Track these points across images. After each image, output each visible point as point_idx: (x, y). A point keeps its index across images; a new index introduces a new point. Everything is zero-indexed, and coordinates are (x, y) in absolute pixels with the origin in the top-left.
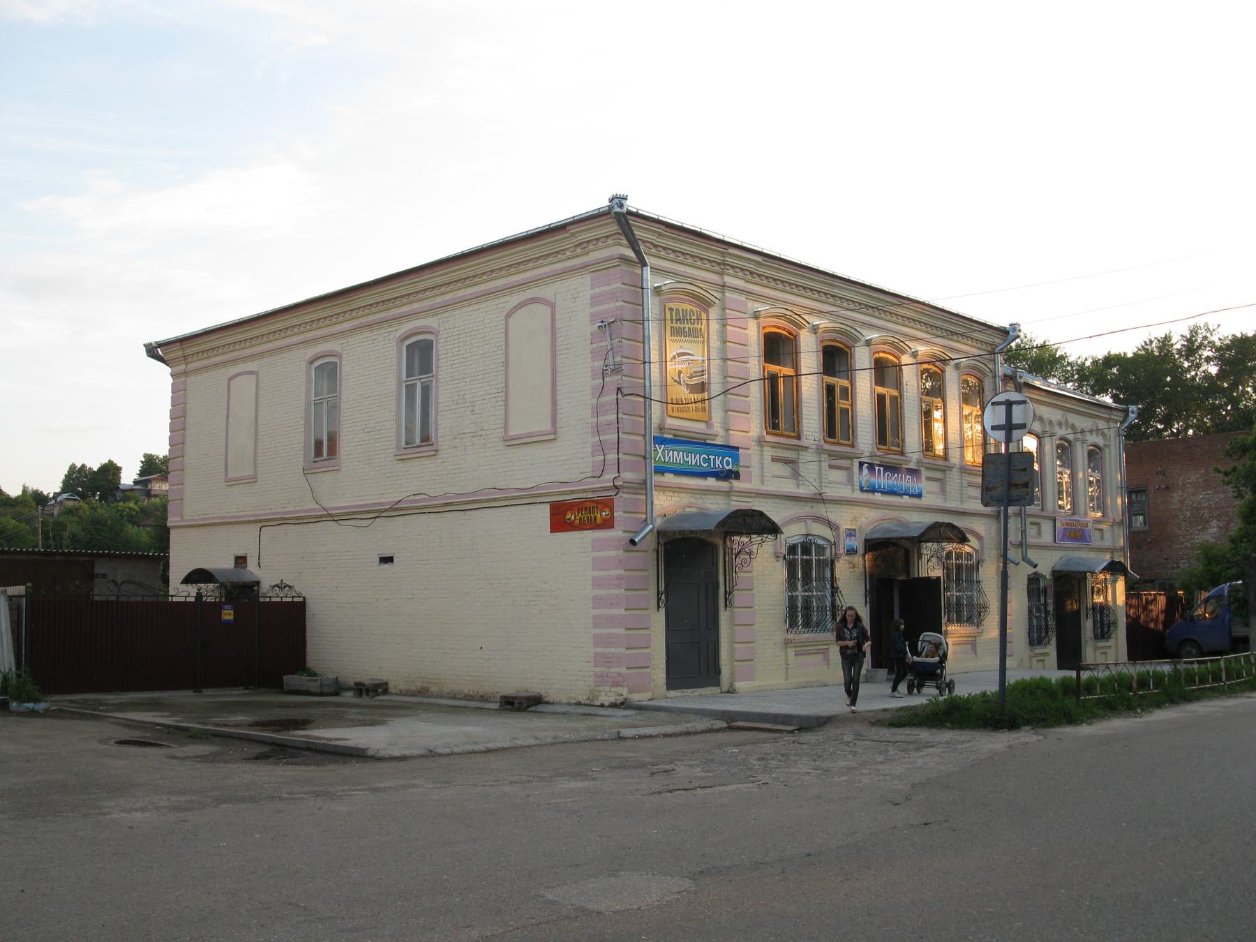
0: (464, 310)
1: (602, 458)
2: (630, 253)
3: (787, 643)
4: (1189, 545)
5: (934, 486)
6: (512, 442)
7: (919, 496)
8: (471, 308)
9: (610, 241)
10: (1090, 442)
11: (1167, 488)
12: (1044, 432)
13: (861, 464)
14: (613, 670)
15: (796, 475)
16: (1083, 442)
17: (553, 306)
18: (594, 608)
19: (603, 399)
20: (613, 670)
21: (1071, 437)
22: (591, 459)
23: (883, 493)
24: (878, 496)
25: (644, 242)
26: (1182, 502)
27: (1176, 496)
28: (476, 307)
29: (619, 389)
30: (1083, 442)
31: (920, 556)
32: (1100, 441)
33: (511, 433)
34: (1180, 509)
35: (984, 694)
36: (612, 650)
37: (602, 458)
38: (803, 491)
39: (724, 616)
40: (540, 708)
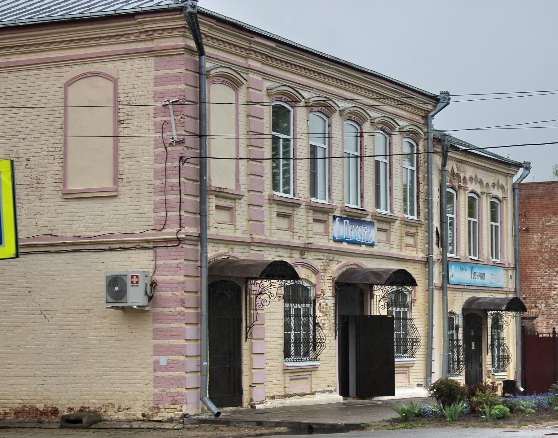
0: (18, 74)
1: (164, 214)
2: (192, 44)
3: (286, 370)
4: (547, 286)
5: (382, 236)
6: (71, 196)
7: (372, 245)
8: (26, 73)
9: (175, 33)
10: (470, 189)
11: (527, 230)
12: (483, 193)
13: (334, 217)
14: (172, 390)
15: (291, 229)
16: (488, 195)
17: (115, 82)
18: (154, 339)
19: (168, 165)
20: (172, 390)
21: (479, 191)
22: (153, 215)
23: (349, 242)
24: (345, 246)
25: (206, 36)
26: (541, 244)
27: (536, 237)
28: (31, 73)
29: (181, 158)
30: (465, 189)
31: (372, 296)
32: (500, 194)
33: (71, 187)
34: (539, 251)
35: (349, 432)
36: (171, 374)
37: (164, 214)
38: (297, 242)
39: (245, 346)
40: (100, 425)
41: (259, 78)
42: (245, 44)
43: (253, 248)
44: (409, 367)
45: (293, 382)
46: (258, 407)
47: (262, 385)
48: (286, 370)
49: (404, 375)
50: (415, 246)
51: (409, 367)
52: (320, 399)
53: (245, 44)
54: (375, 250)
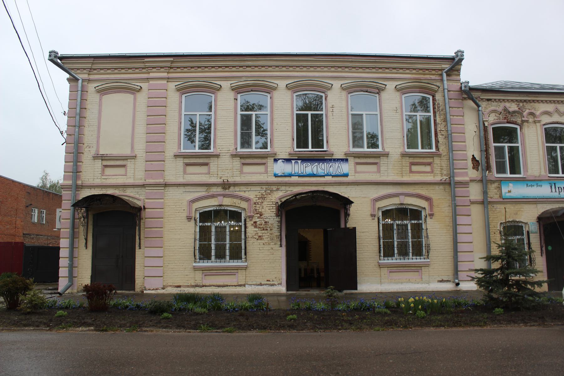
9: (85, 71)
23: (300, 176)
41: (165, 82)
42: (142, 65)
43: (147, 188)
44: (421, 267)
45: (391, 274)
46: (145, 292)
47: (162, 278)
48: (380, 266)
49: (417, 273)
50: (432, 172)
51: (421, 267)
52: (436, 287)
53: (142, 65)
54: (350, 179)
